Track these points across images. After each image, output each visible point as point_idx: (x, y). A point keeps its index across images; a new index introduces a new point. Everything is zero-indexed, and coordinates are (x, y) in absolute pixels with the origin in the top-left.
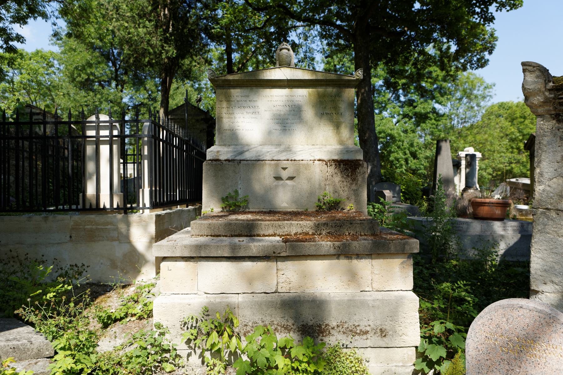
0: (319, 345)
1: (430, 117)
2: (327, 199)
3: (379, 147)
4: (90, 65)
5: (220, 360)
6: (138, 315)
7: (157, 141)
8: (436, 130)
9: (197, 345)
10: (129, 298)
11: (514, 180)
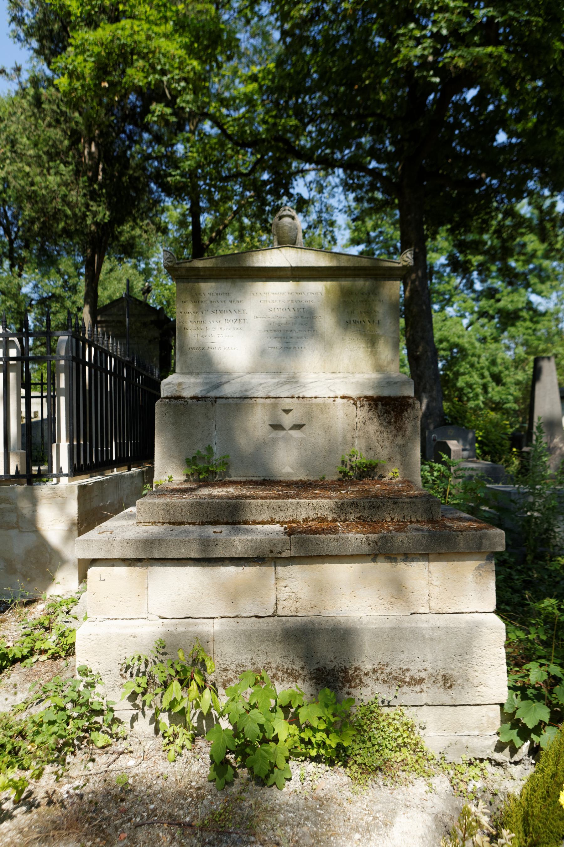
0: (343, 703)
1: (522, 317)
2: (356, 461)
3: (440, 365)
5: (185, 727)
6: (50, 652)
7: (81, 366)
8: (533, 337)
9: (148, 703)
10: (35, 622)
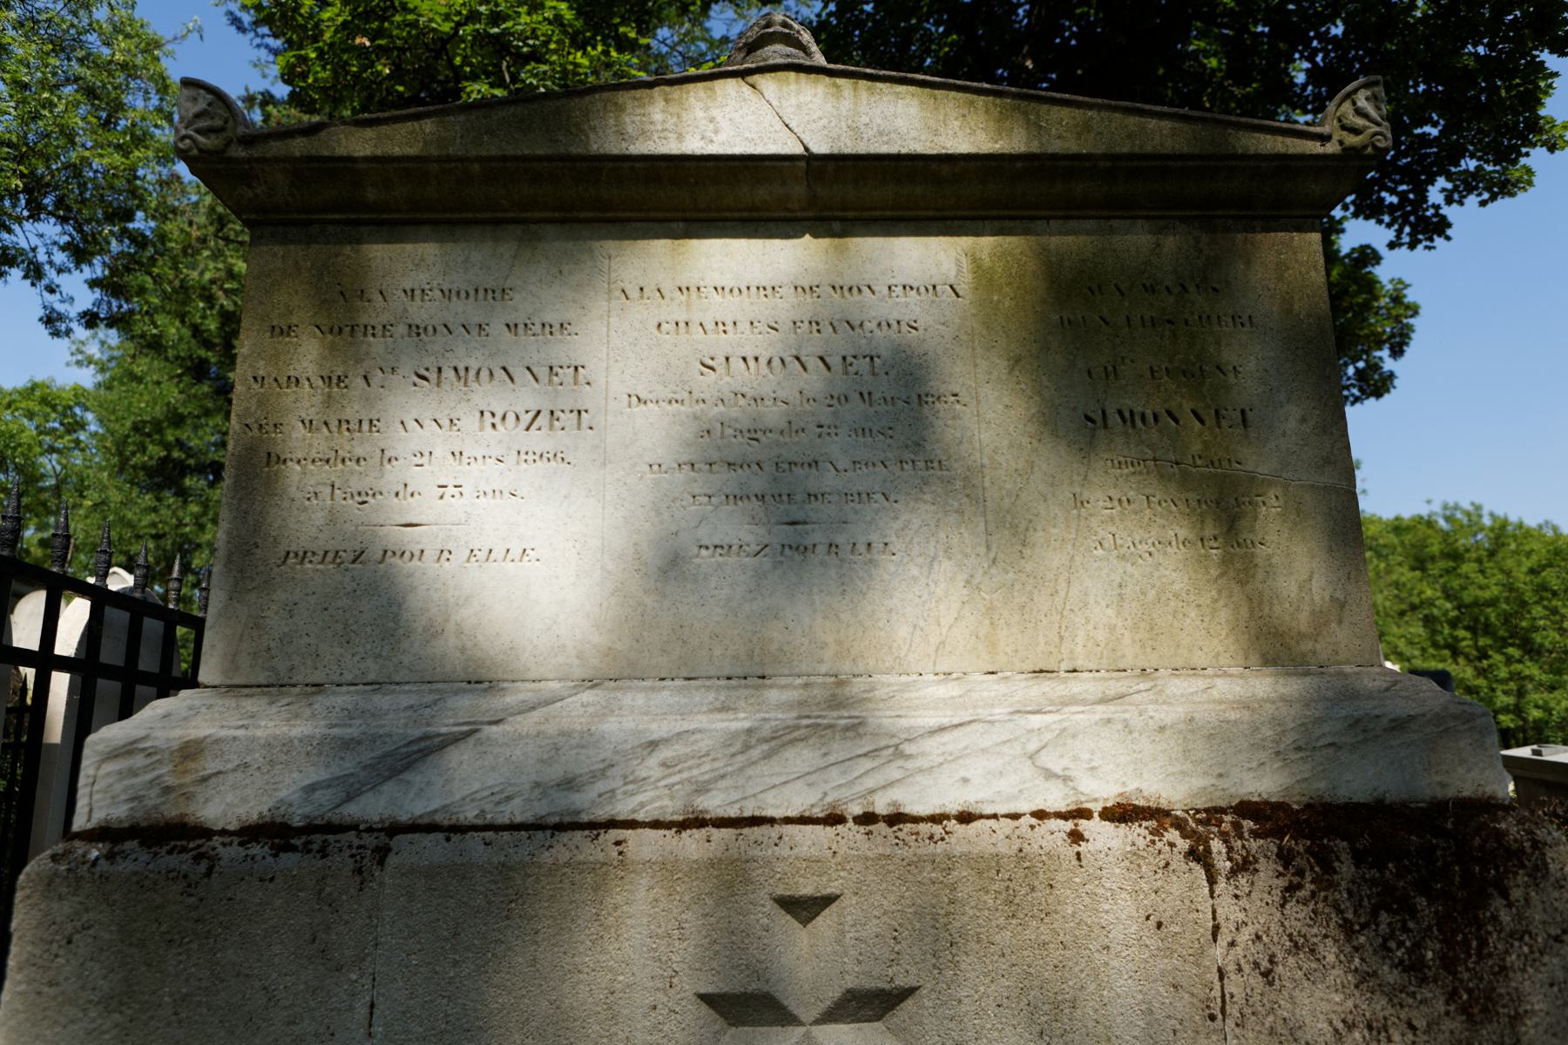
4: (177, 420)
11: (1525, 752)
